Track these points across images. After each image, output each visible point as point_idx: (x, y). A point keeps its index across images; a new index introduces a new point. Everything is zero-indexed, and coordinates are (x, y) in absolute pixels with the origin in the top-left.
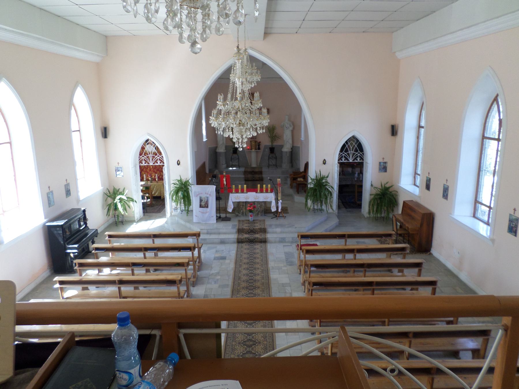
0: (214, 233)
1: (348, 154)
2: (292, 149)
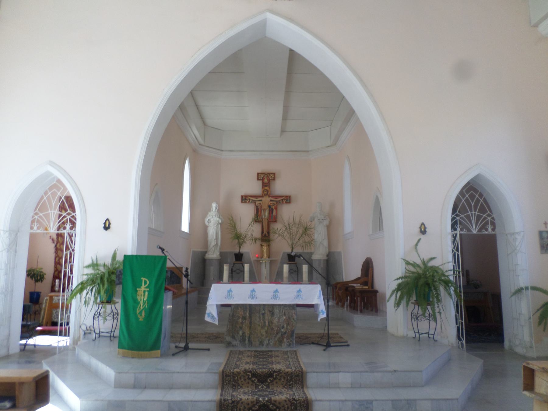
0: (157, 387)
1: (468, 217)
2: (327, 256)
